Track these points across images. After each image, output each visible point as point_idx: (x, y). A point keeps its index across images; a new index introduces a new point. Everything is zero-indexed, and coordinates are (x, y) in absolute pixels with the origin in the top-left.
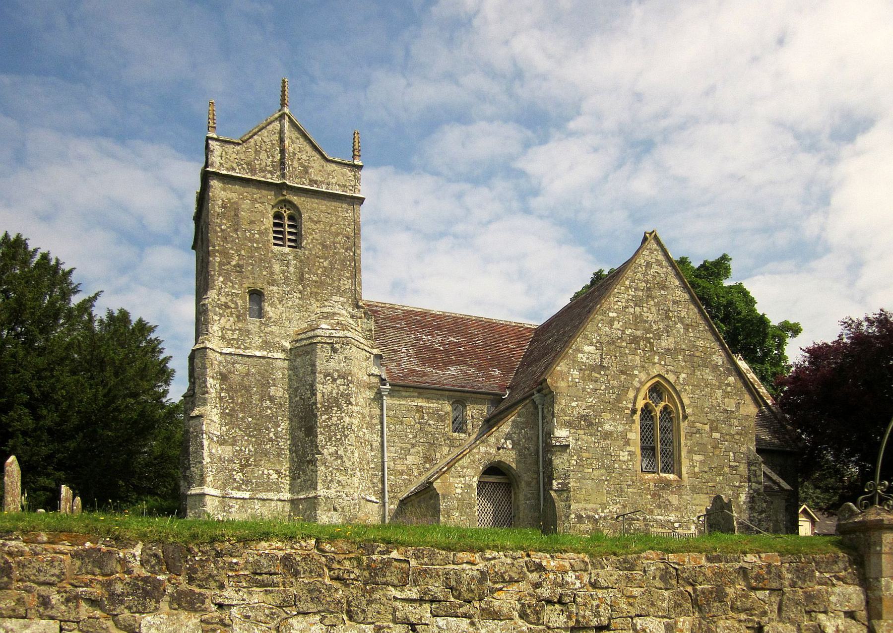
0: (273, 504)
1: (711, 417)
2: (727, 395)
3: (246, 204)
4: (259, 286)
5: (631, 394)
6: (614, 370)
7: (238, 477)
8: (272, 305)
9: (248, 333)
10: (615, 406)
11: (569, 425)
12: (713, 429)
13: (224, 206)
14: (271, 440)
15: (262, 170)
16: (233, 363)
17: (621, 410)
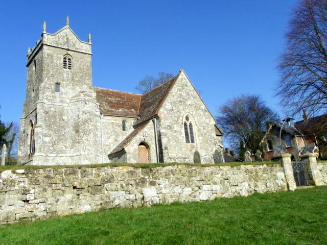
0: (64, 158)
1: (203, 125)
2: (206, 118)
3: (55, 55)
4: (59, 82)
5: (181, 118)
6: (175, 111)
7: (52, 148)
8: (63, 88)
9: (55, 97)
10: (177, 122)
11: (165, 128)
12: (204, 129)
13: (48, 55)
14: (63, 135)
15: (61, 44)
16: (51, 108)
17: (179, 123)
